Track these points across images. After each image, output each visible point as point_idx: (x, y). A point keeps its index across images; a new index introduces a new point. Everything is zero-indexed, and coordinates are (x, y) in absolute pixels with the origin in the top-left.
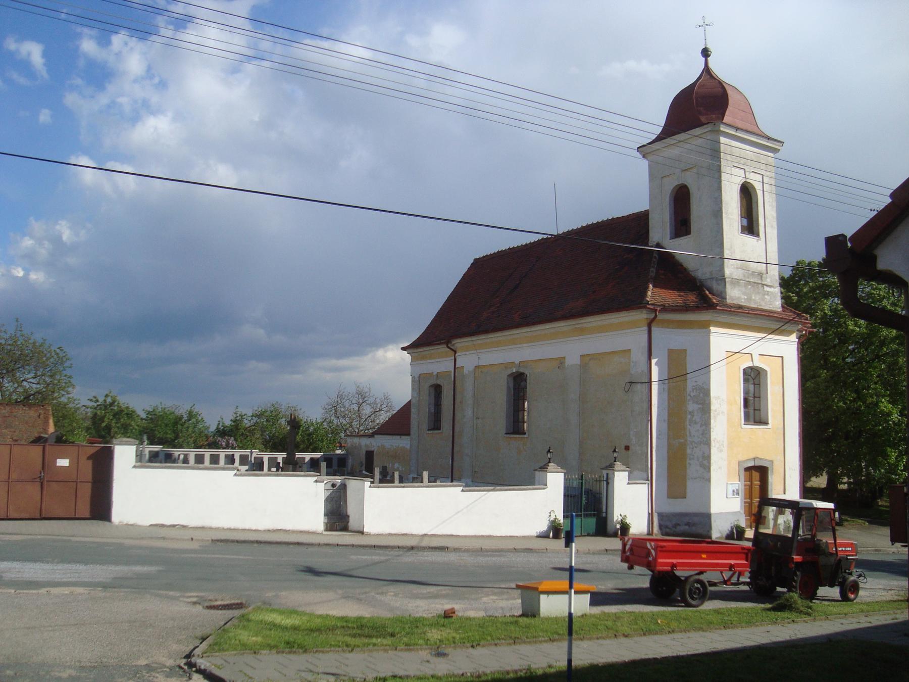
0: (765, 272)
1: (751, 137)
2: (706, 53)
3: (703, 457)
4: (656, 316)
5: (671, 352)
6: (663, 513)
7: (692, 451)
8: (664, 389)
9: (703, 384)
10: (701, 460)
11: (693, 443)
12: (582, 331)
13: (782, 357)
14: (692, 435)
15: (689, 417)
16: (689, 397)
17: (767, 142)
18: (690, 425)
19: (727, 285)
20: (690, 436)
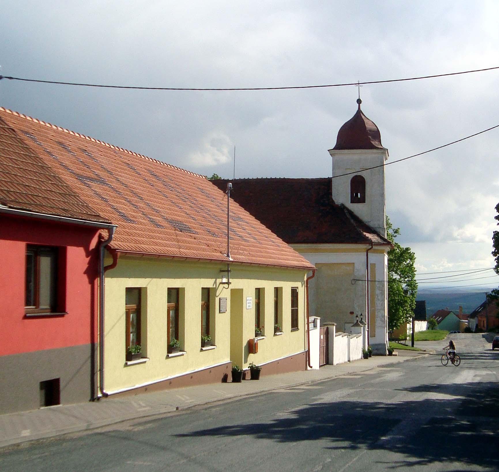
2: (359, 101)
3: (382, 316)
4: (372, 247)
10: (381, 318)
12: (317, 251)
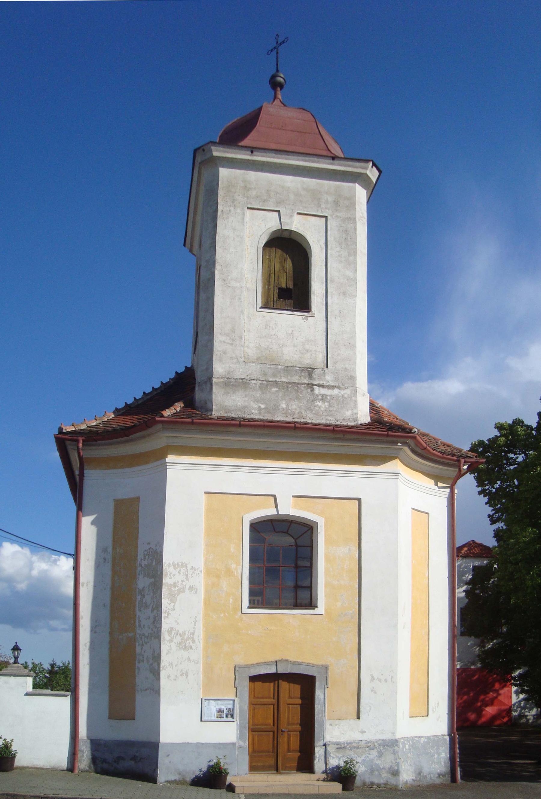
0: (323, 365)
1: (290, 159)
5: (119, 504)
6: (100, 740)
7: (142, 649)
8: (105, 559)
9: (156, 546)
10: (151, 661)
11: (143, 637)
13: (359, 500)
14: (142, 625)
15: (139, 598)
16: (139, 569)
17: (332, 164)
18: (140, 610)
19: (214, 387)
20: (140, 626)
